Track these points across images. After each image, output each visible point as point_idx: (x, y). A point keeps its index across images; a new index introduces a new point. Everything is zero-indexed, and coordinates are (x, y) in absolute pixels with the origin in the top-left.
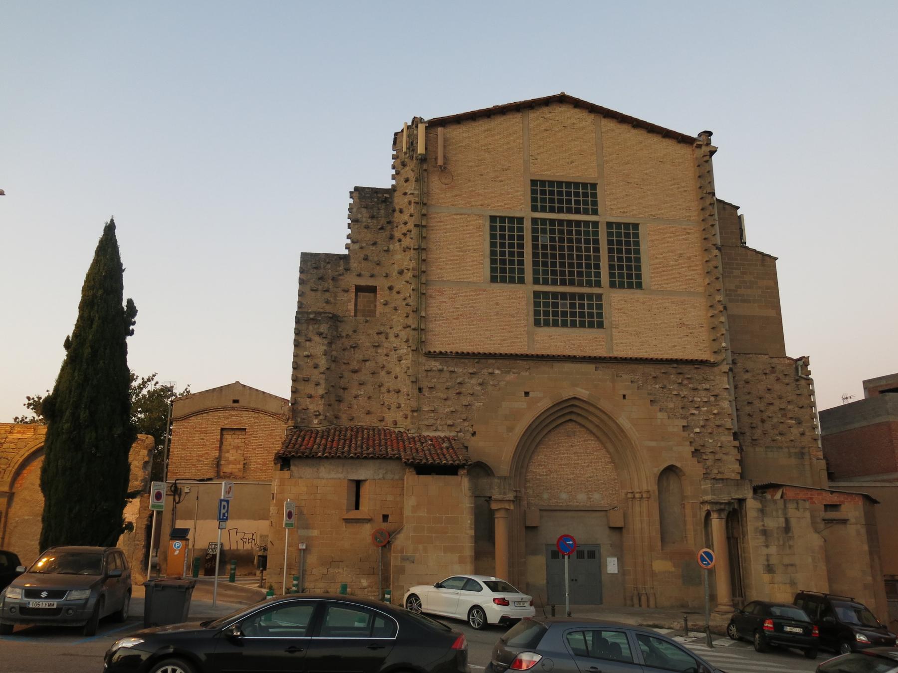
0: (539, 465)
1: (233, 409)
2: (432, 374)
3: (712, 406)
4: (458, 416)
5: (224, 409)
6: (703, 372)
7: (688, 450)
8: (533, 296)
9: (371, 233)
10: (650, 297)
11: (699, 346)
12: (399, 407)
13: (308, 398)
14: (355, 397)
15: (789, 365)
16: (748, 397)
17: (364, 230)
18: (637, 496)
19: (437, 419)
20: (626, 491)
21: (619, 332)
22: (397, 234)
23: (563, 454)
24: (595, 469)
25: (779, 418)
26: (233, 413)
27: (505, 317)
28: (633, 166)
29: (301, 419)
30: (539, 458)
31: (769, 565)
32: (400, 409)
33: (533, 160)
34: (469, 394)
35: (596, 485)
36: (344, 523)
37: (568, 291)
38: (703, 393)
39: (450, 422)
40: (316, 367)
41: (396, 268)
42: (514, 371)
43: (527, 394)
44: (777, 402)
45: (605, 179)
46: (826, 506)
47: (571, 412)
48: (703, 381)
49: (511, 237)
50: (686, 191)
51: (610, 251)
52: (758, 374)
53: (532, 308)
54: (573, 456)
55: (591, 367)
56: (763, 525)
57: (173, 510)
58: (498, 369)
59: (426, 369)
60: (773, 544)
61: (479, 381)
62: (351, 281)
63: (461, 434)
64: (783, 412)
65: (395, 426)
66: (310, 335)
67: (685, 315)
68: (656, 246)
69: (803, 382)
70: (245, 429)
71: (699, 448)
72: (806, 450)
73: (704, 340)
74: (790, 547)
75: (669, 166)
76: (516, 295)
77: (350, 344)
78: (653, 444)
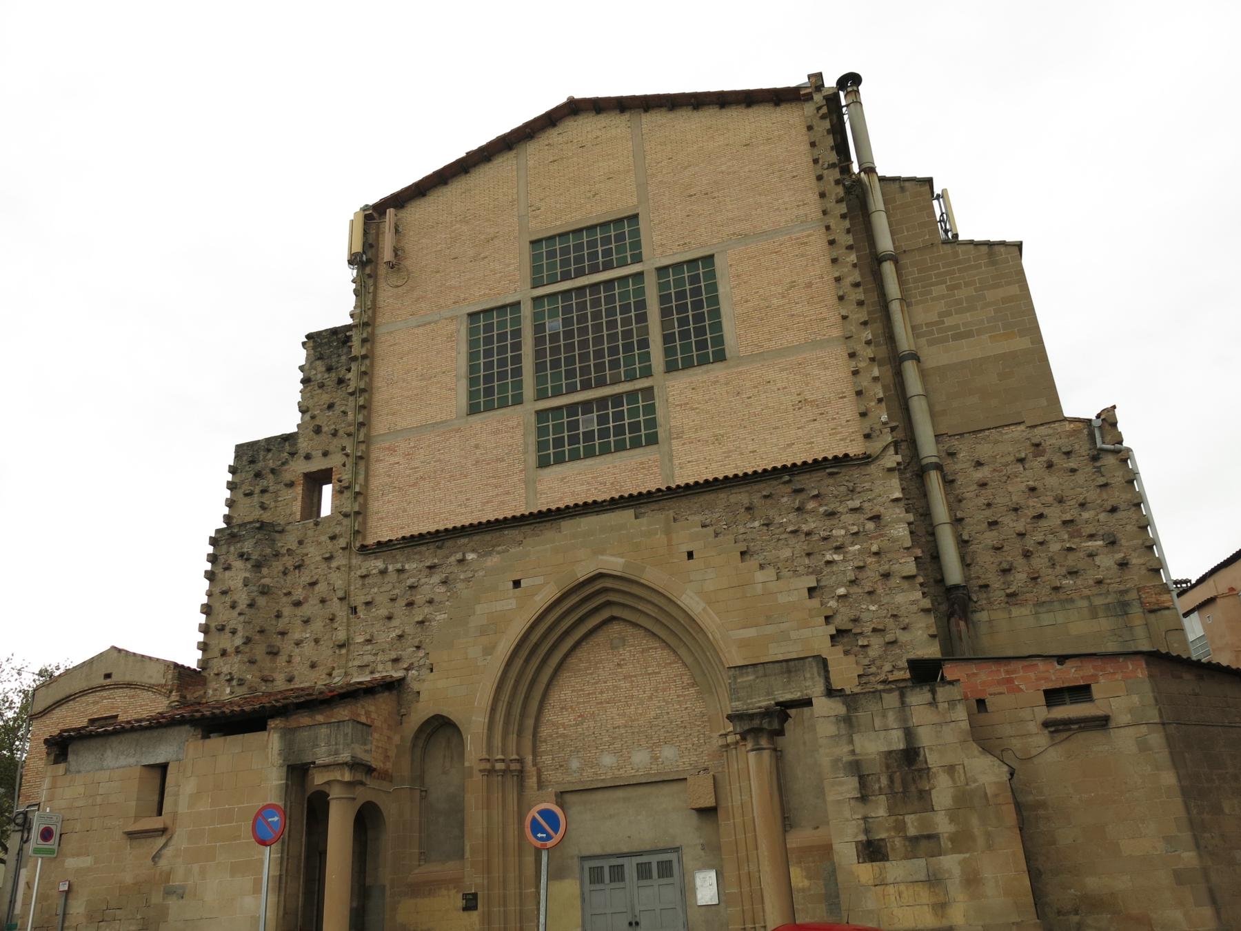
0: (562, 708)
2: (370, 581)
3: (871, 539)
5: (93, 690)
6: (847, 478)
9: (327, 393)
11: (841, 433)
15: (1074, 433)
16: (988, 513)
21: (683, 444)
23: (605, 682)
24: (664, 700)
25: (1064, 541)
26: (105, 694)
27: (488, 464)
28: (697, 168)
30: (563, 697)
33: (533, 211)
37: (593, 397)
38: (848, 518)
42: (499, 548)
43: (517, 584)
45: (651, 201)
46: (1048, 693)
47: (609, 604)
48: (848, 495)
49: (502, 337)
50: (797, 176)
52: (1007, 465)
53: (532, 439)
54: (622, 684)
55: (625, 516)
56: (853, 752)
57: (18, 854)
58: (473, 551)
62: (299, 468)
63: (413, 672)
67: (807, 385)
68: (745, 283)
69: (1110, 460)
70: (686, 779)
71: (849, 626)
73: (848, 421)
75: (762, 148)
78: (751, 633)
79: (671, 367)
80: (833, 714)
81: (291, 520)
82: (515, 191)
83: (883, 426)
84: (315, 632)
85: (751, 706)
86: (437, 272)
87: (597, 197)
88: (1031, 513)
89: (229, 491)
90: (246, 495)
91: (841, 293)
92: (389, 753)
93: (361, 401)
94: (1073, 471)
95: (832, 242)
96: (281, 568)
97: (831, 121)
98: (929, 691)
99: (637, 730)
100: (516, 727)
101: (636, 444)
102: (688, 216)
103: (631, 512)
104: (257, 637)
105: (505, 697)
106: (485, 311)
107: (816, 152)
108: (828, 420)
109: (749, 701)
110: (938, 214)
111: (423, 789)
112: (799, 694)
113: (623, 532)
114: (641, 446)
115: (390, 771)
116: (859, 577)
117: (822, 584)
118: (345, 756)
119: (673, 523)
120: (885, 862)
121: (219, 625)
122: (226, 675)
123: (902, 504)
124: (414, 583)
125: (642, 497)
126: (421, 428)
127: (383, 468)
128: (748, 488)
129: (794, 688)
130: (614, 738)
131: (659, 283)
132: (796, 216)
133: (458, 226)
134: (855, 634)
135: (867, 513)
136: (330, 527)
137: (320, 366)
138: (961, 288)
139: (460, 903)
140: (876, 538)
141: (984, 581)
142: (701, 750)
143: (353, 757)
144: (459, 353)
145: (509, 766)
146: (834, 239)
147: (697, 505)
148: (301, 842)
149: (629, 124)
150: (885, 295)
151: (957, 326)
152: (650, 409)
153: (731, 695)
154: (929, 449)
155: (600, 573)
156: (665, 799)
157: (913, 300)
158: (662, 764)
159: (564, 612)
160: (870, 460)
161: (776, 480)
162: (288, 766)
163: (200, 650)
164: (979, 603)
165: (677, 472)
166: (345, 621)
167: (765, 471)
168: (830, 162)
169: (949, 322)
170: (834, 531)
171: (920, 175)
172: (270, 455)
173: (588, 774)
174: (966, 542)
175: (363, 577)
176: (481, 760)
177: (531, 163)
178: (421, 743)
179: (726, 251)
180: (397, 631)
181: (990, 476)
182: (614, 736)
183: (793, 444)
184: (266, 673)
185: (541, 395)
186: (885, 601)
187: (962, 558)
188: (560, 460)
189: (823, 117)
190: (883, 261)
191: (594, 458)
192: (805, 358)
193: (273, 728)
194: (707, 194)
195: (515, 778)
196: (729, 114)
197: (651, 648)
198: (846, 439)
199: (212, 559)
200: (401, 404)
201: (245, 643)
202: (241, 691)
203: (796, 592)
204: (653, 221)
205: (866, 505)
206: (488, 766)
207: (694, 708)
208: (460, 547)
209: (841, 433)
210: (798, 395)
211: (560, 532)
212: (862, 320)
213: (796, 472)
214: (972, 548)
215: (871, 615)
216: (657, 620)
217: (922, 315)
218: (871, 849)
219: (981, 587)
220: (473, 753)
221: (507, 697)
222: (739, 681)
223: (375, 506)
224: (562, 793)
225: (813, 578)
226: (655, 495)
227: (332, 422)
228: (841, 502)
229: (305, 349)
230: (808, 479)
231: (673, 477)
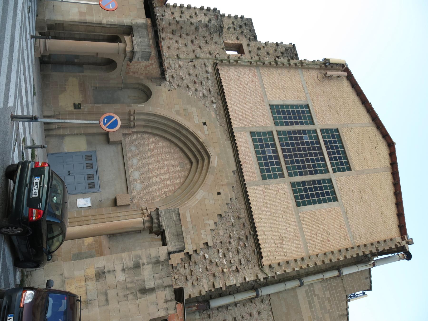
0: (155, 143)
3: (229, 268)
6: (253, 258)
9: (273, 52)
10: (293, 212)
11: (271, 255)
19: (175, 69)
21: (263, 190)
23: (166, 160)
27: (251, 112)
28: (371, 194)
31: (104, 273)
33: (350, 129)
35: (147, 186)
38: (236, 259)
42: (218, 117)
43: (205, 124)
45: (357, 176)
47: (198, 161)
53: (261, 130)
54: (166, 167)
56: (144, 264)
58: (217, 107)
60: (127, 276)
62: (244, 42)
63: (168, 84)
68: (328, 214)
73: (276, 258)
74: (126, 296)
75: (381, 220)
76: (266, 120)
79: (293, 185)
80: (160, 255)
81: (224, 39)
82: (357, 122)
83: (275, 273)
85: (162, 219)
86: (323, 92)
87: (357, 154)
89: (234, 16)
90: (233, 22)
91: (327, 254)
92: (136, 74)
93: (273, 63)
95: (347, 249)
96: (206, 35)
97: (394, 248)
98: (172, 299)
99: (147, 173)
100: (147, 124)
101: (262, 171)
102: (352, 191)
103: (235, 169)
104: (179, 26)
105: (159, 120)
106: (310, 111)
107: (382, 243)
108: (275, 249)
109: (164, 218)
110: (357, 293)
111: (122, 88)
112: (168, 240)
113: (227, 166)
114: (261, 173)
115: (129, 75)
116: (213, 264)
117: (209, 248)
118: (136, 49)
119: (231, 186)
120: (95, 280)
121: (183, 11)
122: (164, 14)
123: (244, 281)
124: (203, 83)
125: (241, 173)
126: (263, 86)
127: (247, 72)
128: (247, 217)
129: (171, 237)
130: (144, 164)
131: (325, 179)
132: (355, 235)
133: (342, 100)
134: (189, 263)
135: (239, 266)
136: (222, 53)
137: (283, 50)
138: (329, 304)
139: (77, 103)
140: (229, 271)
141: (212, 316)
142: (140, 200)
143: (136, 52)
144: (293, 101)
145: (132, 122)
146: (348, 250)
147: (239, 196)
148: (100, 33)
149: (386, 167)
150: (324, 272)
152: (275, 177)
153: (167, 210)
154: (265, 291)
155: (210, 157)
156: (120, 185)
157: (323, 283)
158: (134, 183)
159: (194, 143)
160: (261, 267)
161: (251, 228)
162: (132, 26)
163: (174, 5)
164: (202, 314)
165: (252, 188)
166: (187, 57)
167: (254, 224)
168: (378, 248)
169: (315, 298)
170: (231, 253)
171: (373, 285)
172: (248, 31)
173: (129, 154)
174: (227, 308)
175: (205, 64)
176: (134, 110)
177: (368, 128)
178: (140, 87)
179: (340, 206)
180: (184, 77)
181: (254, 318)
182: (145, 164)
183: (265, 235)
184: (165, 30)
185: (279, 133)
186: (203, 275)
187: (220, 307)
188: (254, 141)
189: (396, 245)
190: (338, 271)
191: (255, 154)
192: (300, 239)
193: (147, 20)
194: (362, 198)
195: (127, 124)
196: (393, 207)
197: (180, 178)
198: (268, 257)
199: (208, 9)
200: (272, 79)
201: (177, 21)
203: (206, 237)
204: (349, 177)
205: (242, 266)
206: (132, 113)
207: (157, 196)
208: (218, 101)
209: (271, 255)
211: (226, 141)
212: (317, 263)
213: (254, 236)
214: (225, 311)
215: (198, 269)
216: (192, 181)
217: (317, 287)
218: (101, 274)
219: (209, 315)
220: (137, 107)
221: (159, 121)
222: (173, 213)
223: (232, 69)
224: (122, 143)
225: (212, 245)
226: (242, 178)
227: (262, 54)
228: (243, 256)
229: (289, 44)
230: (252, 242)
231: (249, 186)
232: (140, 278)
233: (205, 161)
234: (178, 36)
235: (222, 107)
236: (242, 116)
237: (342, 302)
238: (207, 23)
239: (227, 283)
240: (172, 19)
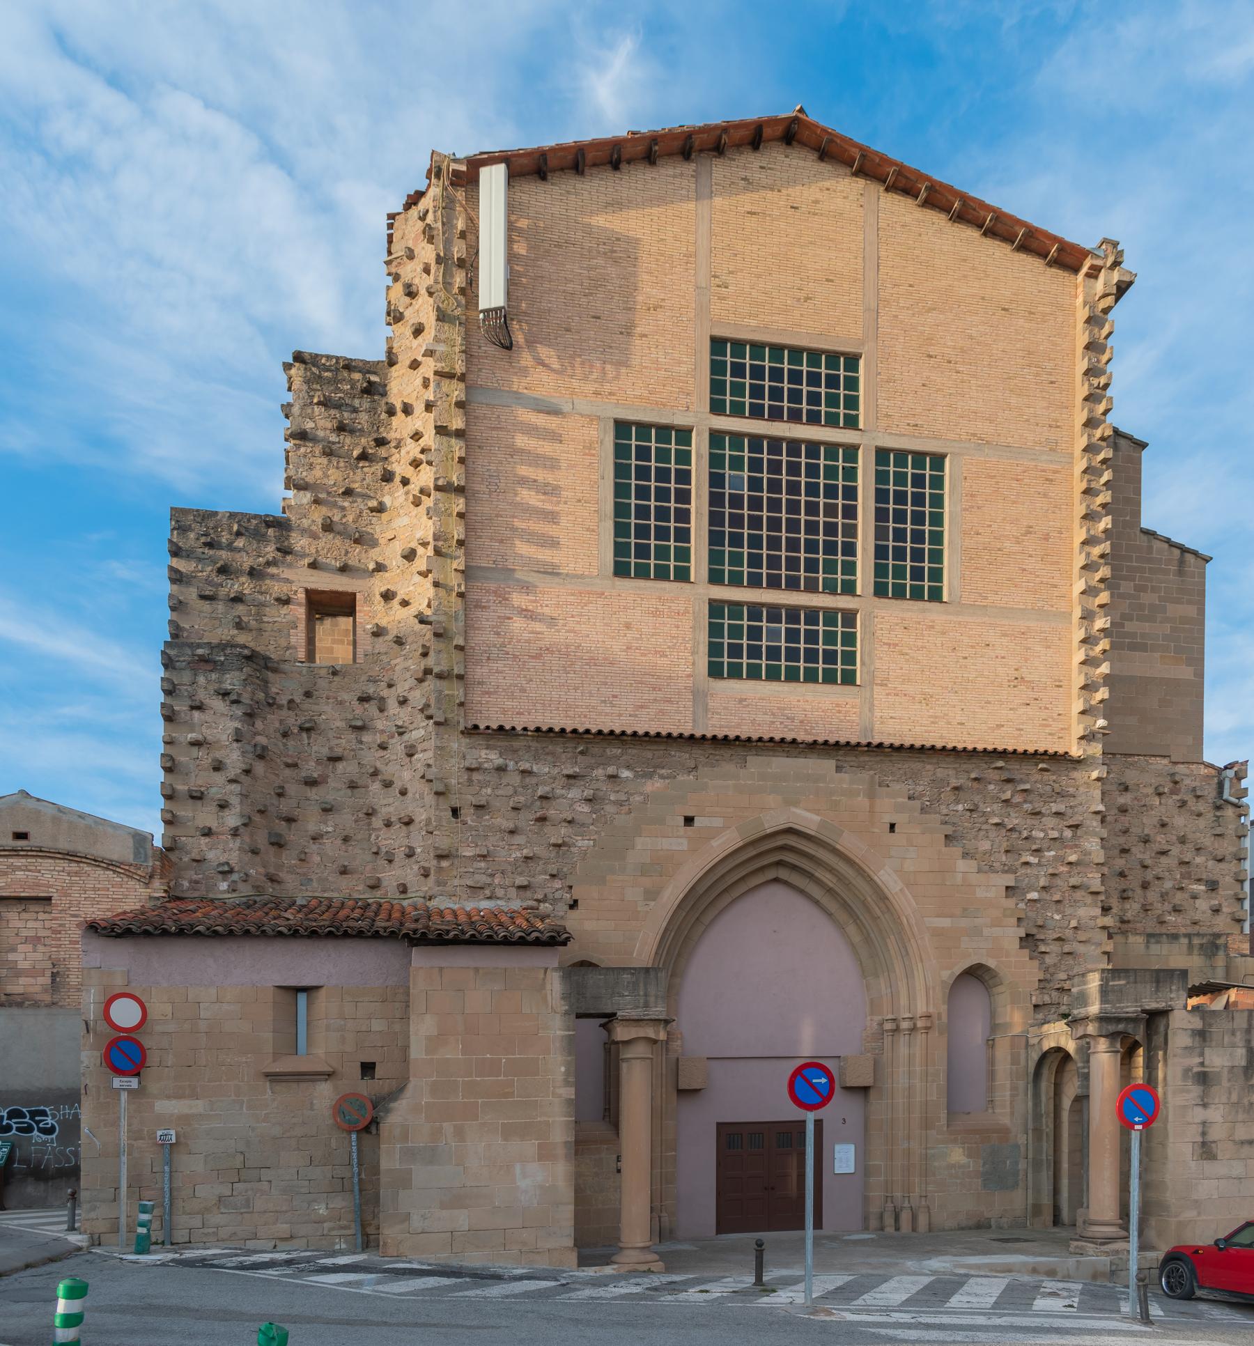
1: (15, 853)
4: (539, 868)
7: (1012, 934)
8: (707, 612)
11: (1050, 726)
12: (410, 854)
13: (204, 835)
14: (314, 839)
16: (1122, 840)
17: (320, 460)
18: (905, 1025)
19: (492, 875)
20: (880, 1018)
21: (888, 694)
22: (400, 467)
25: (1176, 880)
27: (642, 655)
29: (190, 882)
32: (413, 859)
33: (718, 286)
34: (565, 820)
36: (268, 1083)
38: (1050, 822)
39: (521, 880)
40: (218, 767)
41: (399, 547)
42: (663, 771)
43: (689, 821)
44: (1175, 850)
47: (779, 863)
51: (881, 515)
55: (825, 765)
56: (1202, 1064)
58: (628, 767)
59: (467, 764)
60: (1217, 1101)
61: (585, 794)
63: (547, 905)
64: (1184, 869)
65: (402, 896)
66: (202, 695)
69: (1229, 812)
70: (49, 899)
71: (1034, 931)
72: (1221, 941)
77: (299, 722)
78: (945, 922)
84: (341, 827)
88: (1156, 847)
94: (1199, 815)
112: (1164, 1004)
124: (548, 793)
133: (600, 261)
151: (1134, 635)
184: (272, 870)
202: (246, 890)
209: (1050, 726)
210: (1016, 670)
232: (1225, 1071)
233: (794, 844)
234: (290, 830)
235: (630, 751)
236: (654, 689)
237: (1152, 553)
238: (238, 711)
239: (1096, 861)
240: (238, 840)
